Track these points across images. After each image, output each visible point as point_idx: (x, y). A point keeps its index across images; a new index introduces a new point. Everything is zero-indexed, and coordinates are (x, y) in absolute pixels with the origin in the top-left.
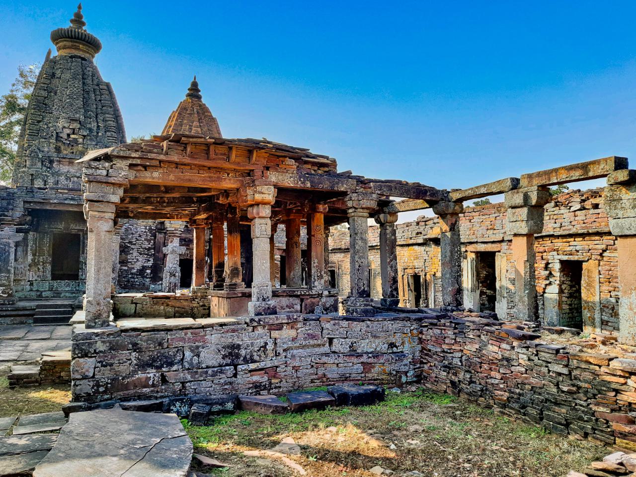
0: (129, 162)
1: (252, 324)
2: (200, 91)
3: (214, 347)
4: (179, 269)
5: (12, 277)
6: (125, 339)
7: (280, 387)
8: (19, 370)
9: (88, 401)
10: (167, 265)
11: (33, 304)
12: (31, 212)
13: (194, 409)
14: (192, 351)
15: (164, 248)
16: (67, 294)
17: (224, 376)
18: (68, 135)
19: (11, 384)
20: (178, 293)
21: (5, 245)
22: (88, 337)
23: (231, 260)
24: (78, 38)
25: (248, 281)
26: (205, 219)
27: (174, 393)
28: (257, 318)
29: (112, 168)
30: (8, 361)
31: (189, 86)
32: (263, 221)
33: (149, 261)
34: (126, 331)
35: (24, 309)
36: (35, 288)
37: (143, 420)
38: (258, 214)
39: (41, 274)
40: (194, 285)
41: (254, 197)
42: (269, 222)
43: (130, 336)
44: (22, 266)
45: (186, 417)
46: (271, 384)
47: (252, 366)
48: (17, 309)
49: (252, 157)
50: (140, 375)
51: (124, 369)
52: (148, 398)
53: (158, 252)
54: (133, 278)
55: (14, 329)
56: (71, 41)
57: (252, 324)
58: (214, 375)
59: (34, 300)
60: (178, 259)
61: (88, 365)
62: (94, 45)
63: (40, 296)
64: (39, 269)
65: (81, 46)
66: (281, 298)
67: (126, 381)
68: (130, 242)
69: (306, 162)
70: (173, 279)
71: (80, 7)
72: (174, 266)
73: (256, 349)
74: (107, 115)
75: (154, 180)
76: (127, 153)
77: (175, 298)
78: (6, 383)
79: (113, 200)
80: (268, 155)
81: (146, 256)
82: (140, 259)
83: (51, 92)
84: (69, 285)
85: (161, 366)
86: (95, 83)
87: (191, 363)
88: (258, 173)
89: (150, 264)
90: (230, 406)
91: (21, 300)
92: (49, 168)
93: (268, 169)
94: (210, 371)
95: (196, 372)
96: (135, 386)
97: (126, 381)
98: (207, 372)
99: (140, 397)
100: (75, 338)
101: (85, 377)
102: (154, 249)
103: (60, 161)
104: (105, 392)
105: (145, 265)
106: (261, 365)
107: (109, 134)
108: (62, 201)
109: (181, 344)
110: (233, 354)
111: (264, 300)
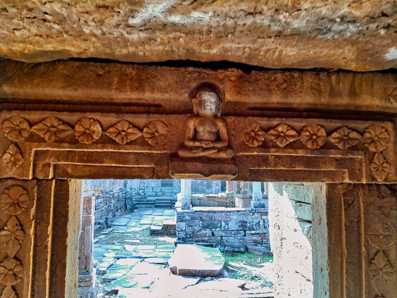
1: (253, 212)
3: (234, 221)
5: (146, 186)
6: (196, 215)
7: (267, 244)
8: (153, 228)
9: (184, 241)
11: (154, 198)
13: (226, 249)
14: (225, 222)
16: (168, 194)
17: (239, 235)
19: (151, 233)
20: (220, 195)
22: (183, 213)
27: (218, 240)
28: (254, 209)
30: (148, 224)
34: (197, 211)
35: (151, 201)
37: (205, 249)
39: (157, 184)
40: (227, 192)
43: (199, 214)
45: (223, 252)
46: (262, 241)
47: (253, 232)
48: (148, 201)
50: (203, 232)
51: (197, 228)
52: (208, 242)
54: (198, 186)
55: (147, 210)
57: (253, 212)
58: (235, 234)
59: (154, 196)
61: (183, 225)
63: (156, 194)
67: (198, 233)
73: (255, 224)
77: (218, 198)
78: (149, 233)
84: (169, 189)
85: (212, 228)
87: (224, 228)
90: (242, 249)
91: (149, 196)
94: (233, 232)
95: (227, 232)
96: (202, 236)
97: (198, 233)
98: (232, 233)
99: (203, 241)
100: (178, 213)
101: (182, 231)
104: (189, 238)
106: (258, 232)
109: (220, 219)
110: (243, 225)
111: (258, 200)
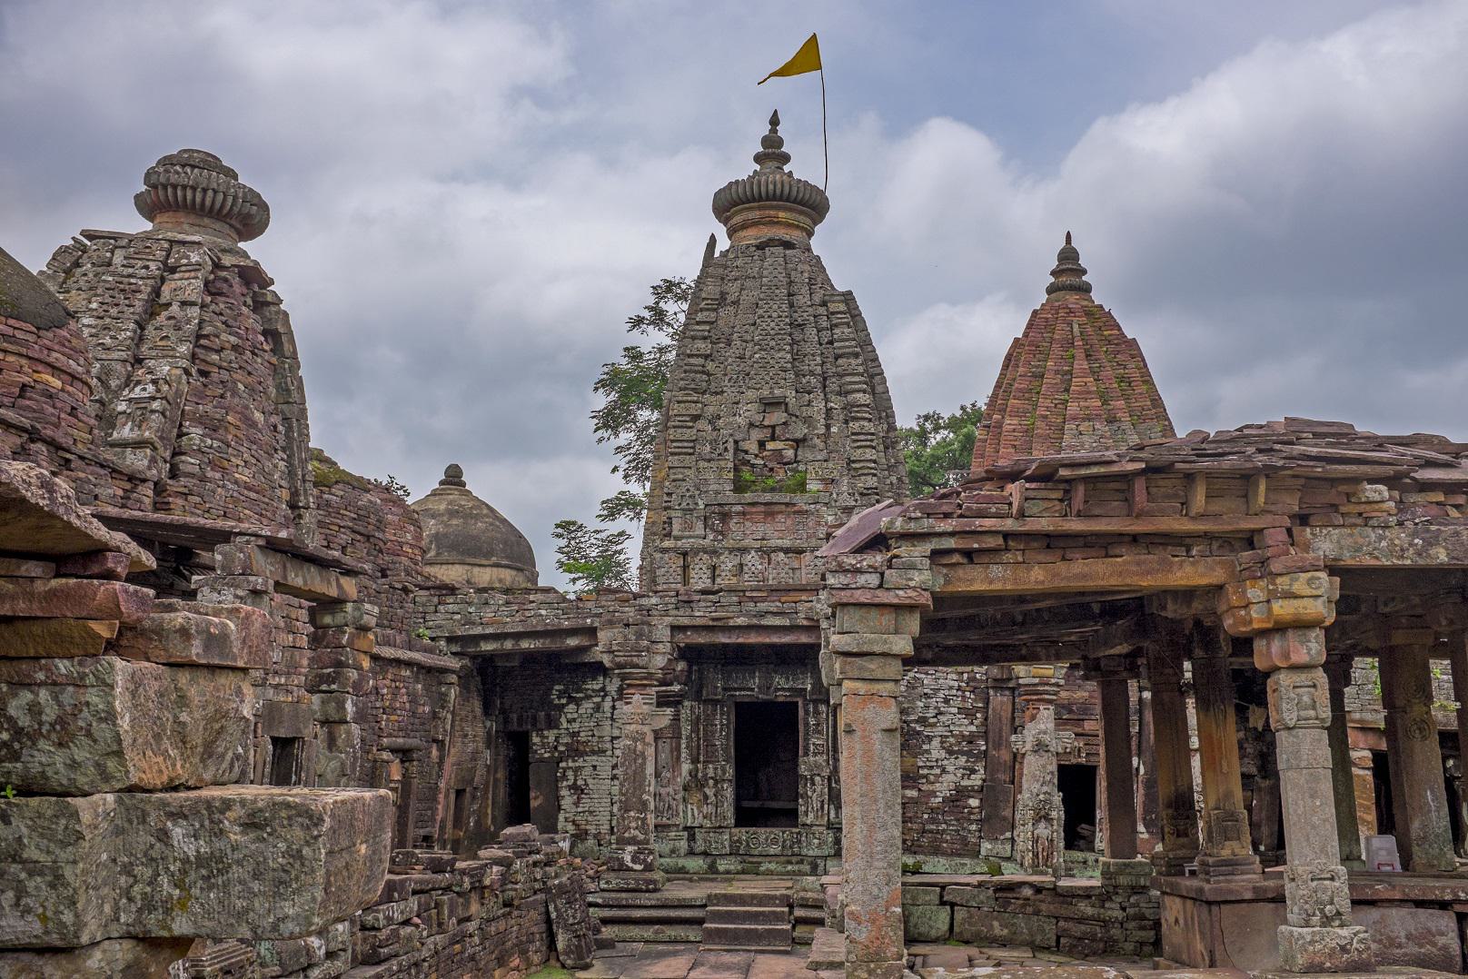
0: (928, 547)
2: (1084, 272)
4: (1057, 798)
10: (1025, 786)
12: (690, 654)
15: (1013, 738)
18: (762, 444)
21: (635, 740)
23: (1210, 781)
24: (774, 198)
25: (1275, 851)
26: (1126, 656)
29: (890, 567)
31: (1054, 264)
32: (1302, 678)
33: (973, 771)
36: (700, 846)
38: (1286, 656)
39: (711, 809)
41: (1270, 610)
42: (1321, 677)
44: (670, 790)
49: (1256, 494)
53: (998, 746)
56: (759, 208)
60: (1054, 768)
62: (812, 205)
63: (712, 869)
64: (706, 797)
65: (781, 214)
66: (1386, 911)
68: (922, 720)
69: (1426, 486)
70: (1043, 830)
71: (774, 121)
72: (1045, 789)
74: (848, 379)
75: (992, 587)
76: (926, 524)
79: (896, 649)
80: (1302, 481)
81: (964, 759)
82: (950, 768)
83: (718, 340)
86: (817, 298)
88: (1276, 537)
89: (976, 781)
92: (721, 533)
93: (1303, 520)
102: (985, 735)
103: (744, 514)
105: (965, 783)
107: (855, 426)
108: (755, 621)
